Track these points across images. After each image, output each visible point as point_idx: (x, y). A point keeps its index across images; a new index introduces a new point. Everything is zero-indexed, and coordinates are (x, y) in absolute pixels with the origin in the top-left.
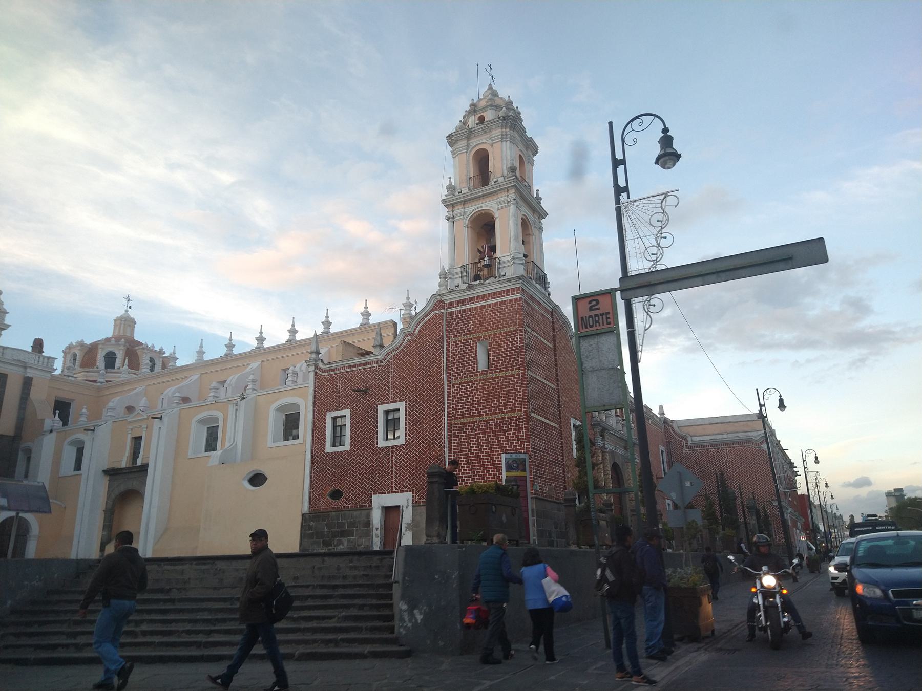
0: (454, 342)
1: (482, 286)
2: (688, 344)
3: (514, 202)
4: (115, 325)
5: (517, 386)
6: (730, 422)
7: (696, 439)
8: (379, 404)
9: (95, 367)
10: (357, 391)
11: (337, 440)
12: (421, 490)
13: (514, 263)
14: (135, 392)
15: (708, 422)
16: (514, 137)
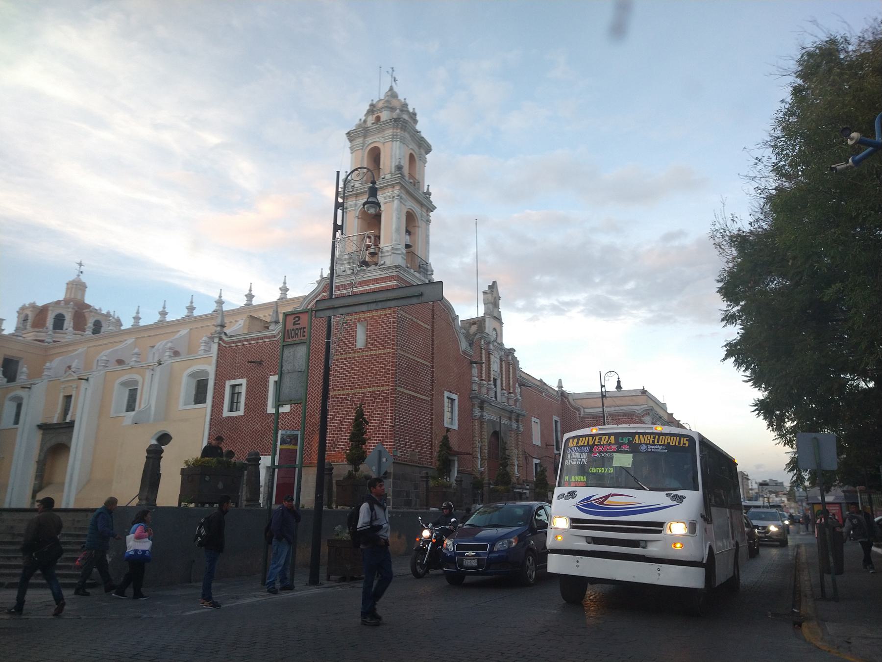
2: (649, 316)
5: (388, 364)
6: (618, 397)
7: (587, 411)
8: (271, 375)
10: (251, 362)
14: (77, 352)
16: (404, 138)
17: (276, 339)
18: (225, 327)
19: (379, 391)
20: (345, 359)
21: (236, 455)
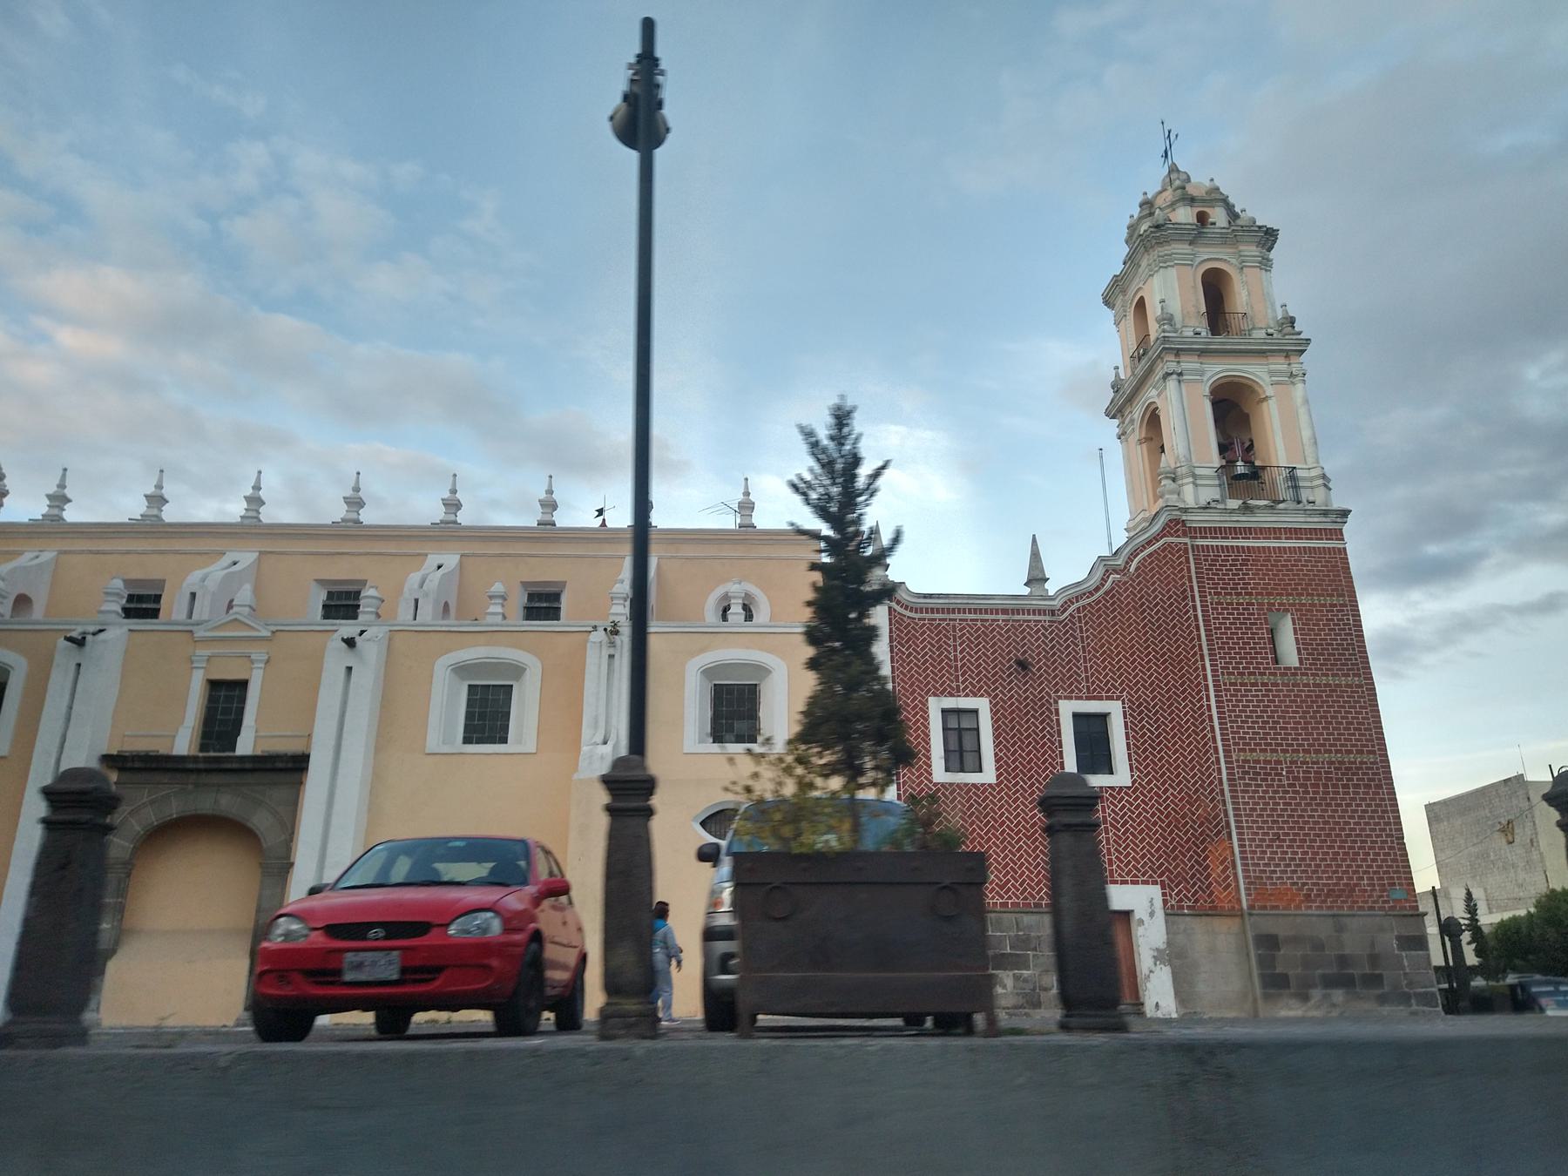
1: (1271, 511)
8: (1060, 698)
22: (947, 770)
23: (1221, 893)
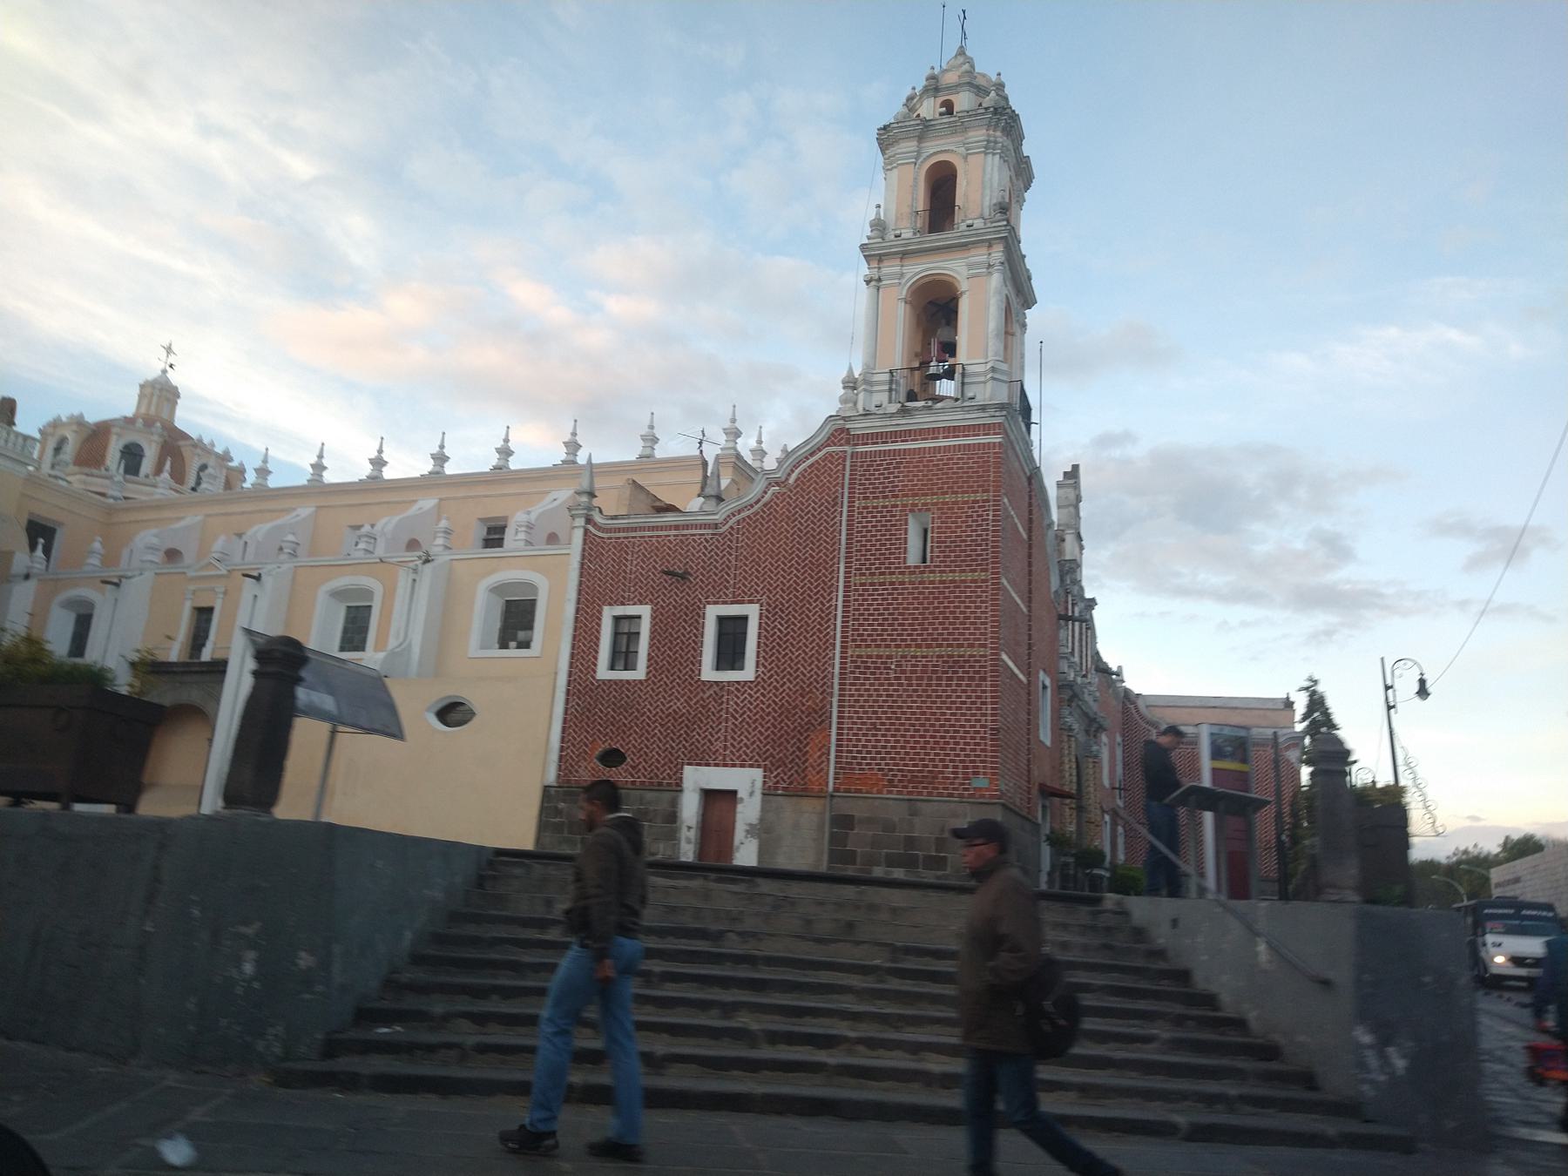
0: (864, 508)
3: (1000, 267)
4: (141, 396)
5: (982, 602)
8: (709, 603)
9: (103, 469)
10: (667, 573)
11: (623, 655)
12: (779, 766)
13: (993, 379)
14: (182, 523)
15: (1198, 704)
17: (721, 531)
18: (596, 497)
19: (963, 656)
20: (881, 584)
21: (629, 760)
22: (742, 668)
23: (814, 777)
